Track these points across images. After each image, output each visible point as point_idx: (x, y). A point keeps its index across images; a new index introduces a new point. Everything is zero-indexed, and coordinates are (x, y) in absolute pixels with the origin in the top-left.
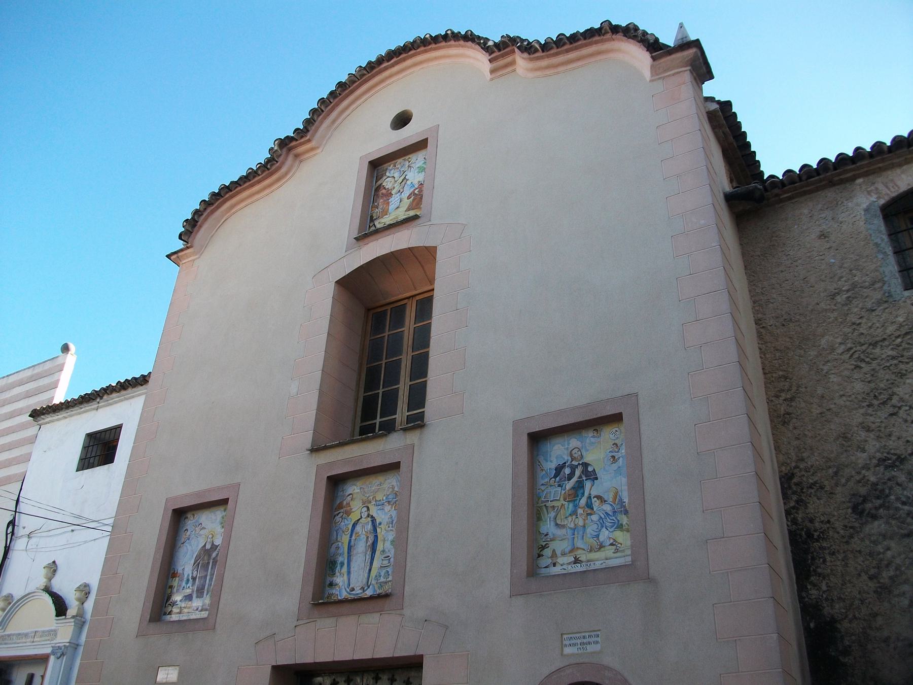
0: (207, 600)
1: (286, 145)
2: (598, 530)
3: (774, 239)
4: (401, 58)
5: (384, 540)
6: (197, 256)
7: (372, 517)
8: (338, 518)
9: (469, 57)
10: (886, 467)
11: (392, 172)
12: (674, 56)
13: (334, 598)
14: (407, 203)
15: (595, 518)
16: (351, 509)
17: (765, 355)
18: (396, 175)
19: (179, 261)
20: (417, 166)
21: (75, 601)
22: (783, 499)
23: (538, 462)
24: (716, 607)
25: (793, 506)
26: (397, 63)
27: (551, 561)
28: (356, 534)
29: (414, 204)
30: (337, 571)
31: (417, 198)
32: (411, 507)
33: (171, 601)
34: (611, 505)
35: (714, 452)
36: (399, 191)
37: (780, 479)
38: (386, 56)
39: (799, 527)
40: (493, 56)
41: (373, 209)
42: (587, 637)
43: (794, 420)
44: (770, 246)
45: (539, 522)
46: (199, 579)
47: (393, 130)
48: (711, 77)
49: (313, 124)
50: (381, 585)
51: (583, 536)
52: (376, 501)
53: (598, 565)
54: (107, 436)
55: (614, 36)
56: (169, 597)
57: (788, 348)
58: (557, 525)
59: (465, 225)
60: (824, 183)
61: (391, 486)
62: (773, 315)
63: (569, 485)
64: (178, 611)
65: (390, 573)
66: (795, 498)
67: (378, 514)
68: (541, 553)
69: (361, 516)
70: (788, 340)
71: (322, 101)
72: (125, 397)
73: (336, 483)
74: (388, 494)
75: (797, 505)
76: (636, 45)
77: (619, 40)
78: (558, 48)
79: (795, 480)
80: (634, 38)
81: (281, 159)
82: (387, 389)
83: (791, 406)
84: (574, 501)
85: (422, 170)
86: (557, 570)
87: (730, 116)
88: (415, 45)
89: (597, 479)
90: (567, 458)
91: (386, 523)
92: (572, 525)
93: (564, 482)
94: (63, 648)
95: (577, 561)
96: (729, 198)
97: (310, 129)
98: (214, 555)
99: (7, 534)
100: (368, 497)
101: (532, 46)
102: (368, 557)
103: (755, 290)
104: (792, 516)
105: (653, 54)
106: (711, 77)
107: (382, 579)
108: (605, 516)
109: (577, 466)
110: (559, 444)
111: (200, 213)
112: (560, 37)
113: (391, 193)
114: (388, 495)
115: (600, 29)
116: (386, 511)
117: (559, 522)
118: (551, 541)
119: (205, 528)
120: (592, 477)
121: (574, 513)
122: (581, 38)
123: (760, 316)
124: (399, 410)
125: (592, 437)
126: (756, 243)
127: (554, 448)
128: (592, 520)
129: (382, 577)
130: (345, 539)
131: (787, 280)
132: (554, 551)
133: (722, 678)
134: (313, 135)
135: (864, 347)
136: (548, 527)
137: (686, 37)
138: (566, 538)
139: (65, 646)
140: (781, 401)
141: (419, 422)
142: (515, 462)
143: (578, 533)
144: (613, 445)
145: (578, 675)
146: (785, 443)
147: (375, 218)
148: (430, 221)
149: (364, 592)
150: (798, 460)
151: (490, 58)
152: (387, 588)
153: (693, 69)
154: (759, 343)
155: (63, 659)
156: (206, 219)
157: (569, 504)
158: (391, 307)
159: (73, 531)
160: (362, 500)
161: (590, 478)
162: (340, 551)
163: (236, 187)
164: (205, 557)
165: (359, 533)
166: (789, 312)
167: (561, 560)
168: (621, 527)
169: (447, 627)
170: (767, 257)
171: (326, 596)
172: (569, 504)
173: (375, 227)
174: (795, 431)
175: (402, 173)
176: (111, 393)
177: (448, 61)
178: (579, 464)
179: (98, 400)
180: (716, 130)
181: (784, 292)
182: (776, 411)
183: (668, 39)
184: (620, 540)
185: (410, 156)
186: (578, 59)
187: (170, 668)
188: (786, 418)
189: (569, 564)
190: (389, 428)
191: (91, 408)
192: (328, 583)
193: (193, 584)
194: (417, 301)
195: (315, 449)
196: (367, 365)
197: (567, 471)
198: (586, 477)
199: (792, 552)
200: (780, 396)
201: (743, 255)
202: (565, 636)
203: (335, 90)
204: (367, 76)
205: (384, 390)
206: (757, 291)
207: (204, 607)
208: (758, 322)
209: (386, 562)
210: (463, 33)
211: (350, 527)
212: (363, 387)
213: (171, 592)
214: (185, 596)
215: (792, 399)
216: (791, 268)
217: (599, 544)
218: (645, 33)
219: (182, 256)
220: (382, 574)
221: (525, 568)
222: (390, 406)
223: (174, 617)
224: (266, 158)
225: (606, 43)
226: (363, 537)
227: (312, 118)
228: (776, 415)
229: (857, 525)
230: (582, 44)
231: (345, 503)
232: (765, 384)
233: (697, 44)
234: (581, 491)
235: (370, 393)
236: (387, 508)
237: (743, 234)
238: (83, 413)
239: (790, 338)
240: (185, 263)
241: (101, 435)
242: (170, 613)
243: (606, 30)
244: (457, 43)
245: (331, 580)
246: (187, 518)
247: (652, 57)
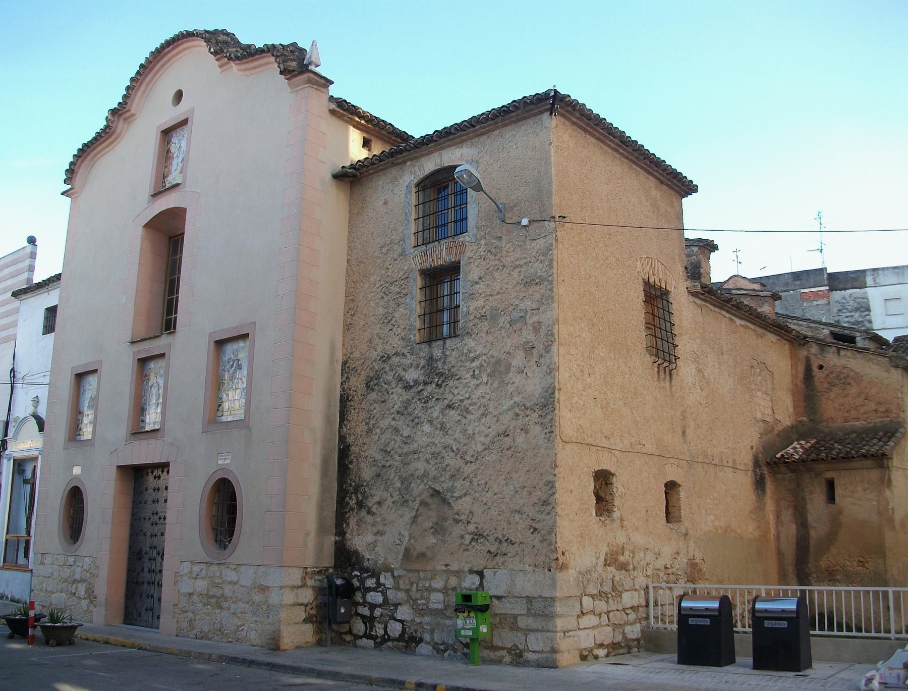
18: (177, 142)
60: (389, 164)
66: (346, 375)
73: (143, 362)
99: (11, 378)
195: (133, 342)
229: (366, 394)
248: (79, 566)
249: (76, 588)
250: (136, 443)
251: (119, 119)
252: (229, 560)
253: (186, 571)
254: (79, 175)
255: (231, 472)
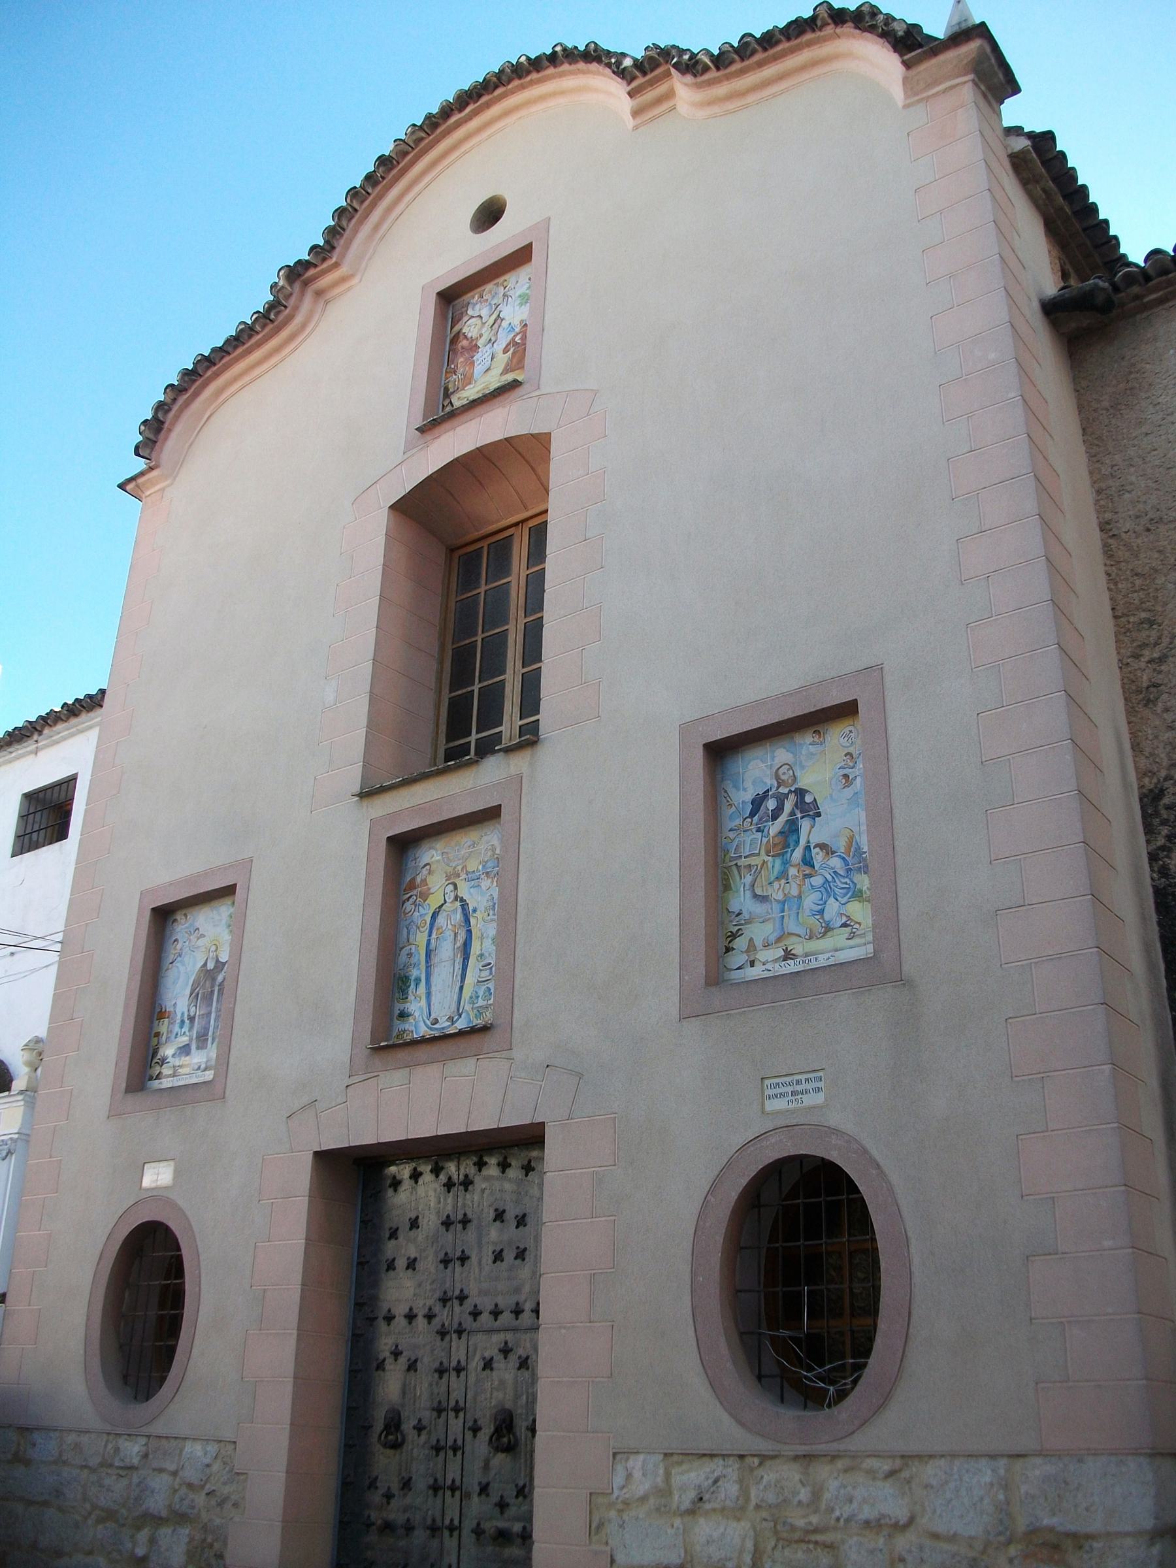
0: (212, 1052)
1: (300, 275)
2: (821, 902)
3: (1132, 376)
4: (481, 104)
5: (482, 938)
6: (168, 482)
7: (462, 900)
8: (409, 906)
9: (596, 90)
11: (477, 307)
12: (942, 58)
13: (408, 1038)
14: (502, 359)
15: (817, 881)
16: (429, 889)
17: (1116, 584)
18: (485, 312)
19: (140, 493)
20: (518, 294)
21: (23, 1066)
22: (1146, 834)
23: (723, 792)
24: (1010, 1023)
25: (1162, 846)
26: (475, 113)
27: (747, 958)
28: (438, 929)
29: (515, 361)
30: (410, 992)
31: (518, 351)
32: (520, 878)
33: (159, 1057)
34: (843, 859)
35: (1009, 759)
36: (490, 340)
37: (1141, 800)
38: (456, 103)
39: (1172, 881)
40: (634, 84)
41: (448, 375)
42: (803, 1082)
43: (1165, 697)
44: (1126, 389)
45: (726, 894)
46: (199, 1019)
47: (476, 233)
48: (1015, 89)
49: (341, 235)
50: (479, 1012)
51: (798, 913)
53: (822, 961)
54: (56, 795)
55: (839, 30)
56: (155, 1052)
57: (1156, 571)
58: (755, 896)
59: (596, 392)
61: (490, 847)
62: (1131, 513)
63: (775, 828)
64: (170, 1072)
65: (492, 991)
66: (1165, 831)
67: (471, 894)
68: (731, 945)
69: (445, 900)
70: (1156, 555)
71: (353, 193)
72: (78, 728)
74: (486, 860)
75: (1168, 844)
76: (877, 43)
77: (848, 36)
78: (742, 60)
79: (1166, 801)
80: (872, 29)
81: (292, 302)
82: (485, 683)
83: (1160, 672)
84: (783, 854)
85: (525, 299)
87: (1051, 159)
88: (504, 78)
89: (819, 814)
90: (770, 782)
91: (484, 909)
92: (780, 896)
93: (766, 824)
94: (9, 1142)
95: (788, 955)
96: (1051, 309)
97: (336, 245)
98: (220, 978)
100: (455, 868)
101: (697, 62)
103: (1099, 470)
104: (1161, 863)
105: (906, 57)
106: (1015, 89)
107: (481, 1002)
108: (833, 877)
109: (787, 796)
110: (757, 759)
111: (166, 407)
112: (745, 40)
113: (476, 345)
114: (486, 862)
115: (813, 19)
116: (484, 888)
117: (759, 892)
118: (746, 923)
119: (205, 936)
120: (811, 813)
122: (782, 38)
123: (1108, 516)
124: (506, 718)
125: (810, 744)
126: (1102, 387)
127: (750, 767)
128: (812, 886)
129: (480, 998)
130: (421, 938)
131: (1156, 450)
132: (751, 940)
133: (1020, 1142)
134: (343, 255)
136: (740, 900)
137: (965, 20)
138: (769, 919)
139: (11, 1139)
140: (1143, 665)
141: (528, 736)
142: (683, 795)
143: (790, 909)
144: (846, 756)
145: (789, 1144)
146: (1150, 737)
147: (451, 390)
148: (539, 388)
149: (452, 1024)
150: (1172, 765)
151: (629, 88)
152: (488, 1017)
153: (979, 78)
154: (1105, 565)
155: (11, 1159)
156: (177, 417)
157: (774, 861)
158: (489, 542)
159: (12, 954)
160: (446, 873)
161: (809, 815)
162: (414, 960)
163: (222, 358)
164: (207, 982)
165: (442, 927)
166: (1158, 507)
167: (763, 955)
168: (859, 894)
169: (580, 1076)
170: (1120, 410)
171: (395, 1034)
172: (774, 861)
173: (453, 406)
174: (1165, 715)
175: (494, 307)
176: (55, 723)
177: (562, 100)
178: (790, 791)
179: (35, 737)
180: (1030, 187)
181: (1149, 471)
182: (1134, 682)
183: (936, 27)
184: (857, 917)
185: (506, 277)
186: (781, 77)
187: (162, 1164)
188: (1151, 693)
189: (776, 961)
190: (486, 749)
191: (27, 752)
192: (397, 1012)
193: (191, 1029)
194: (530, 528)
195: (367, 794)
196: (453, 643)
197: (771, 804)
198: (801, 812)
199: (1160, 924)
200: (1141, 655)
201: (1080, 408)
202: (767, 1082)
203: (374, 171)
204: (427, 141)
205: (481, 685)
206: (1103, 472)
207: (209, 1064)
208: (1104, 526)
210: (582, 48)
211: (428, 919)
212: (448, 682)
213: (158, 1043)
214: (180, 1048)
215: (1162, 660)
216: (1162, 427)
217: (823, 925)
218: (889, 19)
219: (144, 483)
220: (481, 993)
221: (702, 970)
222: (492, 713)
223: (166, 1083)
224: (267, 302)
225: (827, 43)
226: (449, 934)
227: (338, 224)
228: (1134, 688)
230: (784, 50)
231: (418, 880)
232: (1116, 636)
233: (982, 31)
234: (795, 837)
235: (460, 692)
236: (485, 883)
237: (1080, 372)
238: (14, 761)
239: (1159, 551)
240: (149, 495)
241: (45, 794)
242: (158, 1077)
243: (823, 19)
244: (574, 67)
245: (402, 1008)
246: (175, 920)
247: (904, 63)
248: (161, 1470)
249: (152, 1541)
250: (396, 1078)
251: (303, 293)
252: (857, 1443)
253: (641, 1486)
254: (174, 435)
255: (835, 1131)
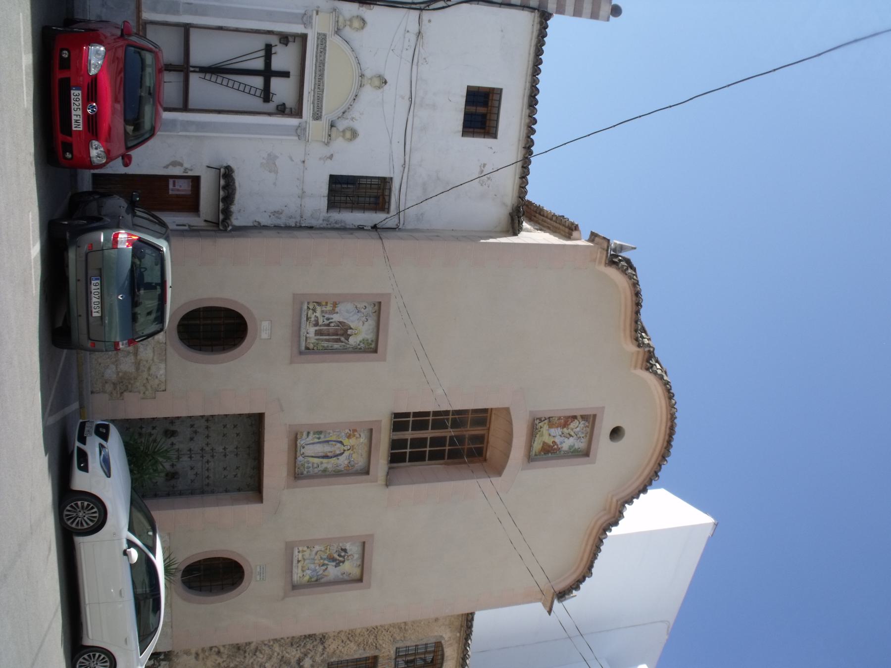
10: (321, 639)
15: (317, 567)
52: (352, 454)
63: (336, 556)
86: (296, 552)
95: (299, 561)
102: (321, 454)
107: (306, 465)
121: (321, 558)
135: (376, 633)
189: (298, 558)
197: (343, 554)
209: (315, 465)
226: (333, 449)
236: (346, 462)
